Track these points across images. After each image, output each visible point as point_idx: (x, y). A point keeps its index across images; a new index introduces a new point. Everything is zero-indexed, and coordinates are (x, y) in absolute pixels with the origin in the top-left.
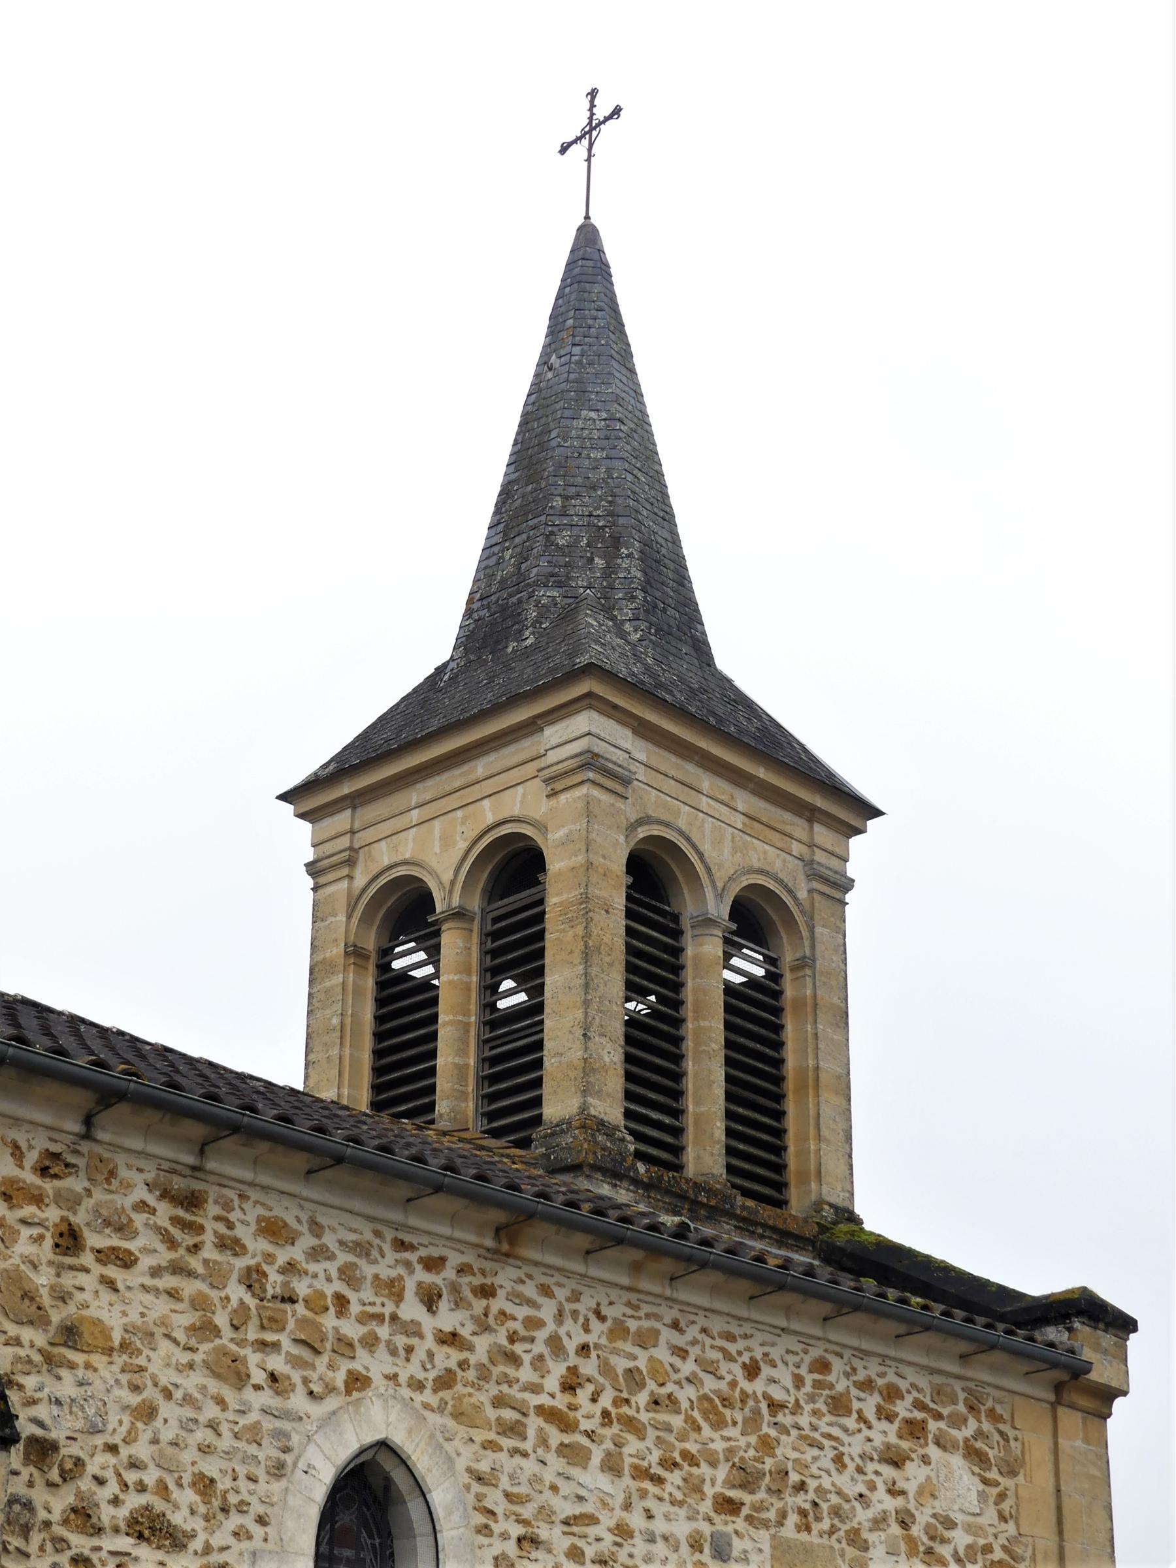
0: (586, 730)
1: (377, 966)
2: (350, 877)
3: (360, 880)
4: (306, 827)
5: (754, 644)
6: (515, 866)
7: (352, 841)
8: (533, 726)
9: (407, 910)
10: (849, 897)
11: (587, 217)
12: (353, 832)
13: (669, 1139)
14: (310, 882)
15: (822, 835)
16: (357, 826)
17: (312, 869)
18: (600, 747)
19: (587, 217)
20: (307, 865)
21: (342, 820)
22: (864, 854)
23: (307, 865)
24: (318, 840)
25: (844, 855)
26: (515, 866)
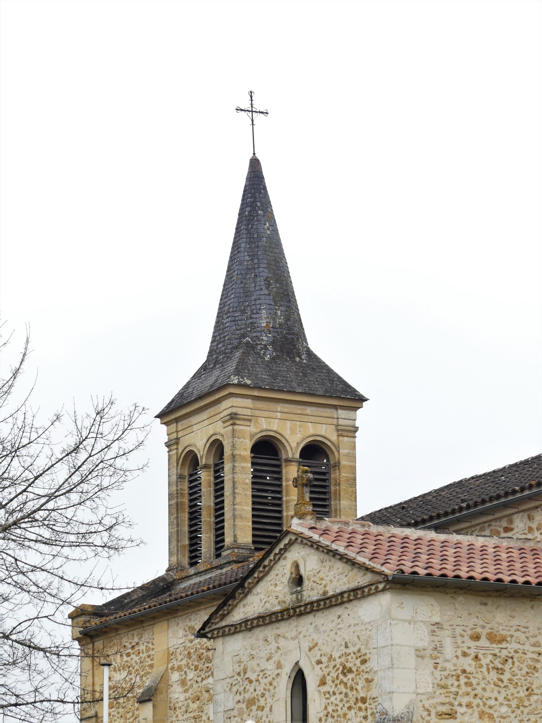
0: (230, 405)
1: (189, 481)
2: (177, 449)
3: (180, 449)
4: (164, 427)
5: (323, 340)
6: (217, 447)
7: (177, 435)
8: (218, 402)
9: (190, 461)
10: (357, 434)
11: (254, 154)
12: (177, 432)
13: (278, 528)
14: (167, 449)
15: (342, 413)
16: (179, 429)
17: (168, 445)
18: (234, 410)
19: (254, 154)
20: (165, 443)
21: (173, 427)
22: (362, 416)
23: (165, 443)
24: (170, 432)
25: (355, 418)
26: (217, 447)
